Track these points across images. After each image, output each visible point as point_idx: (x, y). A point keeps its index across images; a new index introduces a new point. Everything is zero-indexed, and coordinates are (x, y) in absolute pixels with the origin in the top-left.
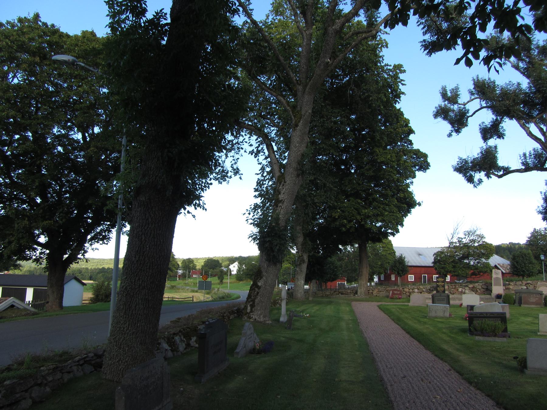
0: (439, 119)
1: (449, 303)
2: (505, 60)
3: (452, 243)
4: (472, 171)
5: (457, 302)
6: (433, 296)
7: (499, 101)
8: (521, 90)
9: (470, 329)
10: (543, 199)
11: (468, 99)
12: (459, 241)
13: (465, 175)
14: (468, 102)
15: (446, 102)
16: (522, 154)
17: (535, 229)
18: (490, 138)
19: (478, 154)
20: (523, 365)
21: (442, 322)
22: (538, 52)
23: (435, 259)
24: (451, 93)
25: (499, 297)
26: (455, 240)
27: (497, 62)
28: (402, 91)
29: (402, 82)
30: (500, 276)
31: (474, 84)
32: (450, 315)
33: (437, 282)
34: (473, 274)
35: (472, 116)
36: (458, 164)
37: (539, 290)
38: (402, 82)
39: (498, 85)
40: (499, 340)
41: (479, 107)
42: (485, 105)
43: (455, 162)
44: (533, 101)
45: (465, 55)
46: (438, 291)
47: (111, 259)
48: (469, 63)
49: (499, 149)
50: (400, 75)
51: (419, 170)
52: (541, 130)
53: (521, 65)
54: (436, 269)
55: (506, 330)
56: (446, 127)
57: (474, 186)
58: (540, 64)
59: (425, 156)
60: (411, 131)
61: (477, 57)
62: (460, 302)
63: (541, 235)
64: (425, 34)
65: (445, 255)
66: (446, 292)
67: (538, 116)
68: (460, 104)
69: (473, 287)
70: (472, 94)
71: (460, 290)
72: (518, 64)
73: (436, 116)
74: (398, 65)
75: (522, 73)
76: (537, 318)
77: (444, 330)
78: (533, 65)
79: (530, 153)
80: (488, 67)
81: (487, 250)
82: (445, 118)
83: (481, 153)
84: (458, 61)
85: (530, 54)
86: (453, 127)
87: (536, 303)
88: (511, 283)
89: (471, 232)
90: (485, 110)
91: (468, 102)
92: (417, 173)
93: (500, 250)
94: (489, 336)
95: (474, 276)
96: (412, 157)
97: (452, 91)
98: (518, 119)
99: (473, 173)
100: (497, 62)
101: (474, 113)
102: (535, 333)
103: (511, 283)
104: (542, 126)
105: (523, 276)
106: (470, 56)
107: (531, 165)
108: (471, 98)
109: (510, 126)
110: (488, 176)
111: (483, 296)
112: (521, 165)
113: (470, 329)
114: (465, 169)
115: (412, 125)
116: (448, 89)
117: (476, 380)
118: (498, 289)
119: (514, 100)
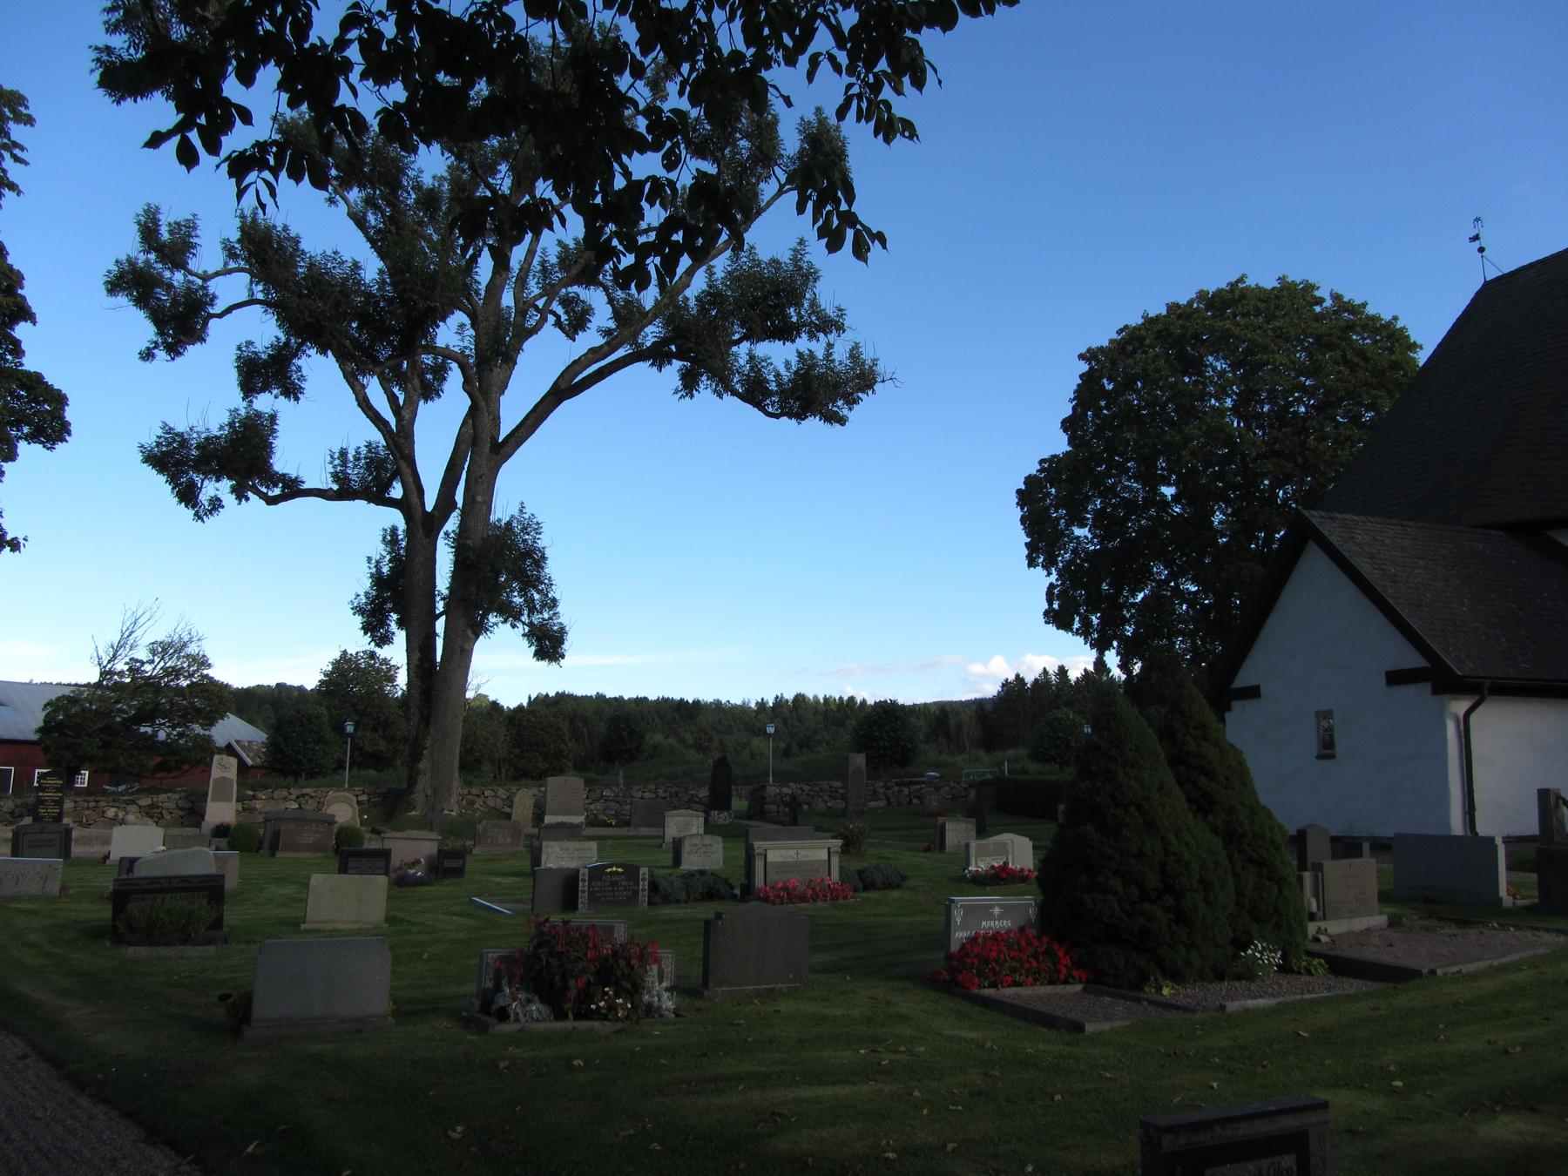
0: (122, 300)
1: (66, 853)
2: (336, 191)
3: (111, 673)
4: (198, 471)
5: (96, 850)
6: (16, 834)
7: (300, 296)
8: (358, 283)
9: (114, 927)
10: (372, 576)
11: (219, 266)
12: (130, 670)
13: (173, 480)
14: (217, 274)
15: (152, 256)
16: (336, 450)
17: (345, 652)
18: (263, 390)
19: (221, 428)
20: (240, 1010)
21: (33, 913)
22: (417, 202)
23: (47, 719)
24: (171, 232)
25: (221, 831)
26: (120, 666)
27: (266, 181)
28: (12, 177)
29: (17, 151)
30: (232, 773)
31: (242, 229)
32: (63, 889)
33: (41, 788)
34: (163, 767)
35: (220, 316)
36: (159, 444)
37: (330, 811)
38: (17, 151)
39: (304, 253)
40: (194, 955)
41: (244, 297)
42: (260, 296)
43: (150, 436)
44: (382, 321)
45: (181, 128)
46: (38, 819)
47: (1449, 829)
48: (187, 157)
49: (281, 426)
50: (11, 124)
51: (31, 438)
52: (392, 399)
53: (371, 218)
54: (47, 750)
55: (217, 924)
56: (143, 329)
57: (196, 514)
58: (414, 232)
59: (59, 400)
60: (24, 313)
61: (213, 147)
62: (105, 849)
63: (358, 668)
64: (113, 28)
65: (83, 710)
66: (66, 820)
67: (390, 363)
68: (191, 273)
69: (152, 806)
70: (231, 253)
71: (111, 813)
72: (365, 214)
73: (116, 285)
74: (13, 93)
75: (369, 239)
76: (306, 885)
77: (32, 937)
78: (398, 228)
79: (358, 453)
80: (238, 184)
81: (209, 699)
82: (142, 302)
83: (231, 425)
84: (156, 140)
85: (397, 198)
86: (161, 333)
87: (314, 848)
88: (260, 795)
89: (170, 645)
90: (258, 308)
91: (217, 274)
92: (22, 447)
93: (251, 702)
94: (166, 944)
95: (164, 775)
96: (11, 394)
97: (176, 228)
98: (342, 358)
99: (198, 479)
100: (266, 181)
101: (229, 310)
102: (294, 924)
103: (260, 795)
104: (396, 390)
105: (297, 775)
106: (194, 136)
107: (356, 486)
108: (226, 264)
109: (319, 370)
110: (240, 493)
111: (176, 831)
112: (330, 479)
113: (114, 927)
114: (178, 463)
115: (31, 292)
116: (166, 219)
117: (100, 1076)
118: (221, 812)
119: (337, 305)
